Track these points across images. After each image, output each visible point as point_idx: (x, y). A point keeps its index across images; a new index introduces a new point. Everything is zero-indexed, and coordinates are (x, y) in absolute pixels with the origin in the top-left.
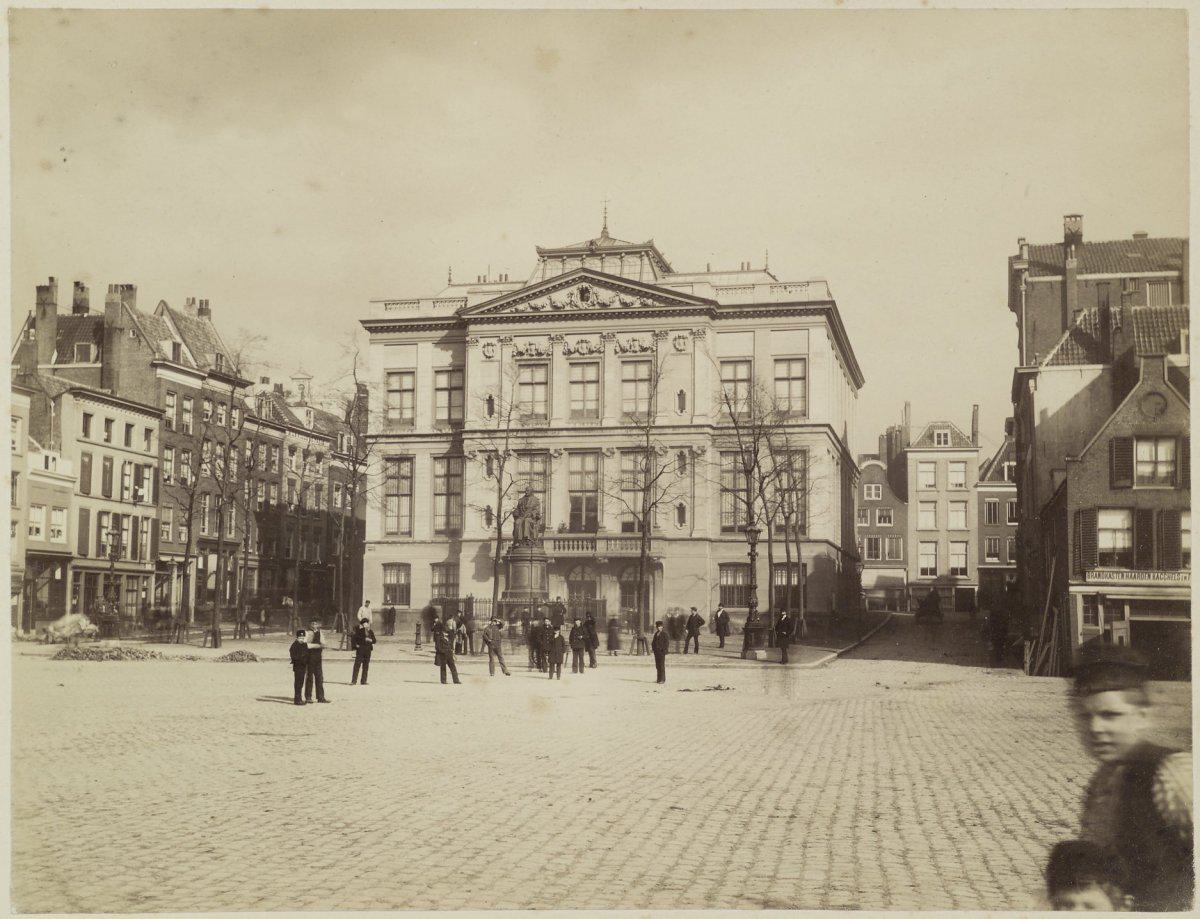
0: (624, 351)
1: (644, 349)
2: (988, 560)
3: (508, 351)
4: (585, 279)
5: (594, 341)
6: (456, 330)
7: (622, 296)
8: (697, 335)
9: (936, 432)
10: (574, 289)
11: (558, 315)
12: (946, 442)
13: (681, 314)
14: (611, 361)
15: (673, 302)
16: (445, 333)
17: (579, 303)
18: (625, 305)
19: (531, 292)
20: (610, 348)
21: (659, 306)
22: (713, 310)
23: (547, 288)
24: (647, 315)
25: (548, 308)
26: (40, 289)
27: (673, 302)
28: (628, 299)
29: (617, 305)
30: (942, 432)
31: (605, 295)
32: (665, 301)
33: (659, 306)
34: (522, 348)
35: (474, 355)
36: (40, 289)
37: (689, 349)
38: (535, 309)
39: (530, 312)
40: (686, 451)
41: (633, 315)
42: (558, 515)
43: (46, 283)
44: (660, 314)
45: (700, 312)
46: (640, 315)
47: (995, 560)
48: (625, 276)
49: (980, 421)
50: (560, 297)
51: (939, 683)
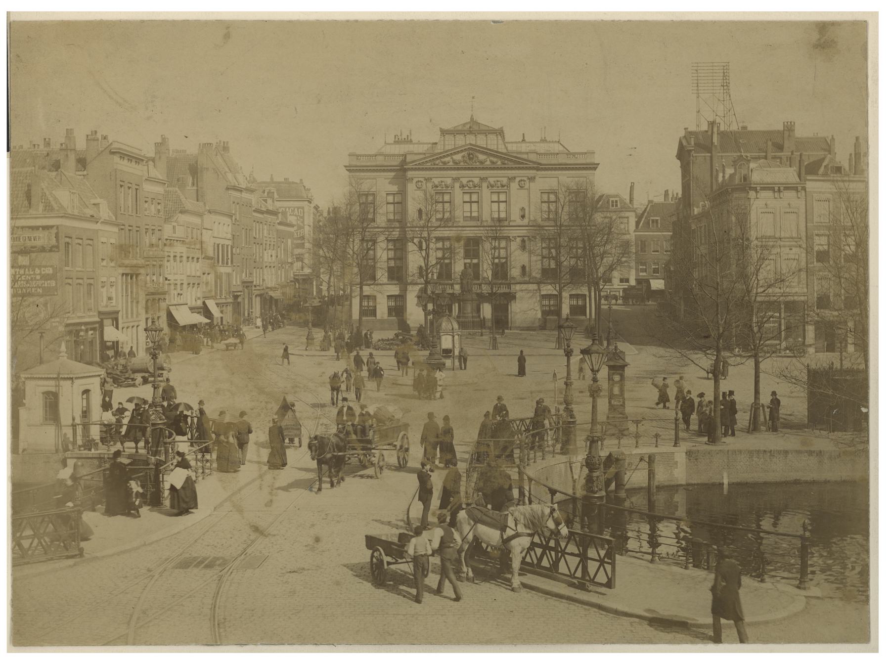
0: (492, 186)
1: (503, 186)
2: (641, 274)
3: (430, 185)
7: (492, 158)
8: (532, 179)
9: (611, 199)
12: (617, 206)
13: (523, 169)
14: (486, 192)
15: (519, 163)
16: (393, 174)
18: (493, 163)
20: (485, 185)
21: (511, 165)
24: (505, 169)
25: (451, 163)
26: (157, 145)
27: (519, 163)
28: (495, 160)
29: (488, 163)
30: (614, 199)
31: (482, 157)
32: (515, 162)
33: (511, 165)
34: (437, 183)
35: (411, 187)
36: (157, 145)
37: (527, 186)
38: (444, 163)
39: (441, 165)
40: (526, 238)
41: (498, 169)
42: (487, 272)
43: (159, 140)
44: (512, 169)
45: (533, 168)
46: (501, 169)
47: (644, 274)
48: (489, 147)
49: (635, 192)
50: (458, 157)
51: (528, 329)
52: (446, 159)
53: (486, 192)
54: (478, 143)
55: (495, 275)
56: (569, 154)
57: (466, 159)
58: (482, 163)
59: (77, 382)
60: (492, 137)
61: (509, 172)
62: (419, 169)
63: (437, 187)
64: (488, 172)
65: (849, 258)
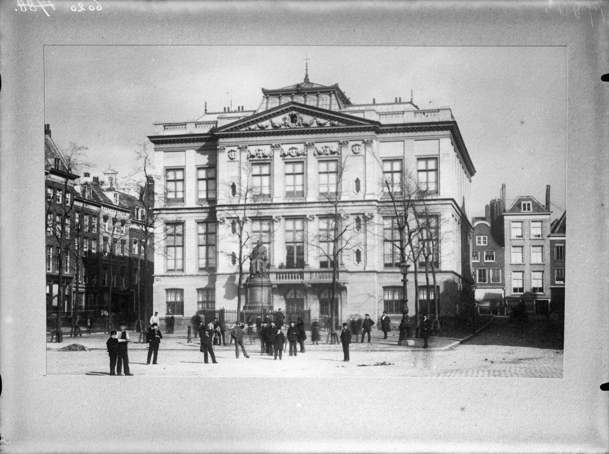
0: (320, 154)
1: (333, 153)
4: (294, 109)
5: (301, 148)
6: (210, 143)
9: (523, 203)
10: (287, 115)
11: (277, 131)
13: (356, 130)
14: (312, 161)
17: (290, 124)
18: (320, 125)
19: (257, 117)
21: (343, 126)
22: (377, 128)
23: (270, 114)
28: (322, 121)
29: (315, 125)
30: (526, 203)
31: (307, 119)
34: (253, 153)
37: (362, 152)
38: (262, 128)
39: (258, 130)
40: (361, 217)
41: (325, 131)
44: (343, 131)
46: (330, 131)
50: (278, 120)
52: (264, 124)
53: (312, 161)
54: (308, 103)
55: (290, 263)
56: (417, 111)
57: (288, 121)
58: (306, 125)
59: (362, 270)
60: (325, 97)
61: (341, 135)
62: (231, 136)
63: (253, 156)
64: (314, 136)
65: (51, 213)
